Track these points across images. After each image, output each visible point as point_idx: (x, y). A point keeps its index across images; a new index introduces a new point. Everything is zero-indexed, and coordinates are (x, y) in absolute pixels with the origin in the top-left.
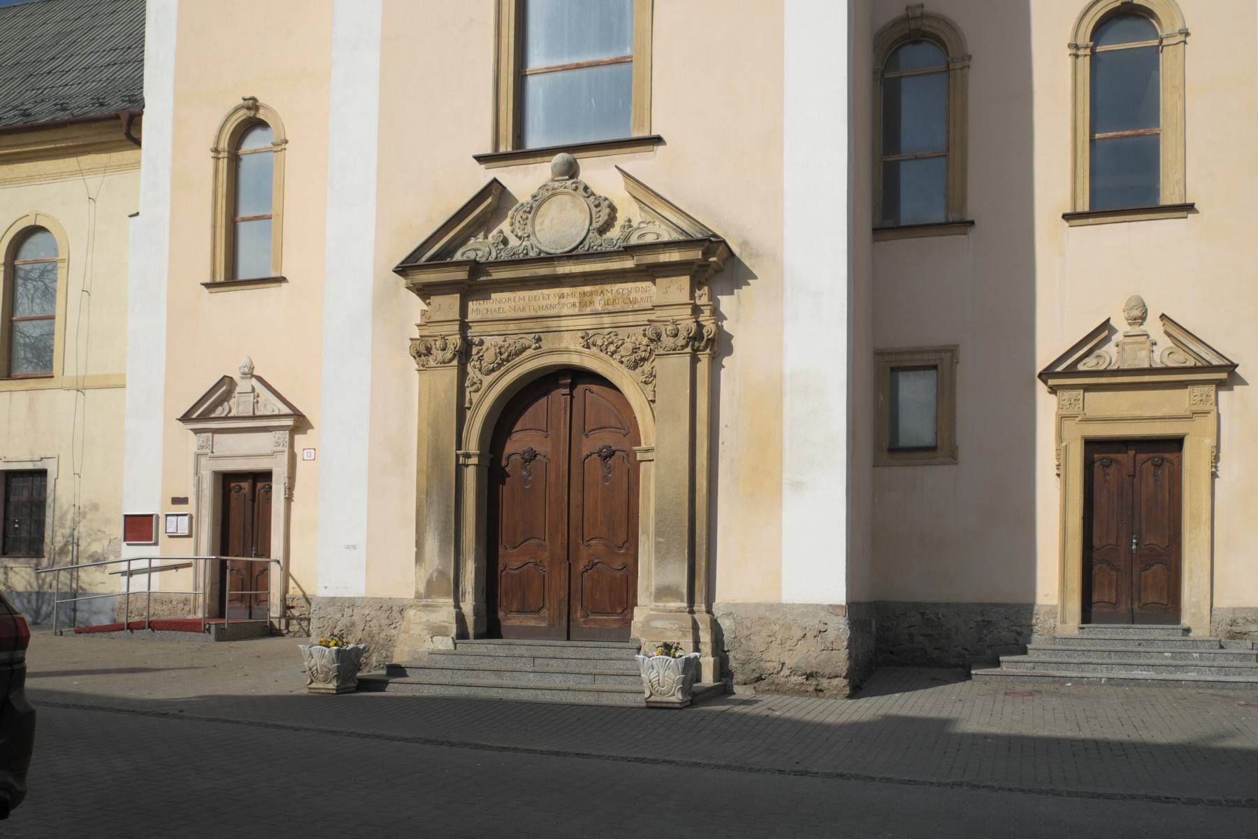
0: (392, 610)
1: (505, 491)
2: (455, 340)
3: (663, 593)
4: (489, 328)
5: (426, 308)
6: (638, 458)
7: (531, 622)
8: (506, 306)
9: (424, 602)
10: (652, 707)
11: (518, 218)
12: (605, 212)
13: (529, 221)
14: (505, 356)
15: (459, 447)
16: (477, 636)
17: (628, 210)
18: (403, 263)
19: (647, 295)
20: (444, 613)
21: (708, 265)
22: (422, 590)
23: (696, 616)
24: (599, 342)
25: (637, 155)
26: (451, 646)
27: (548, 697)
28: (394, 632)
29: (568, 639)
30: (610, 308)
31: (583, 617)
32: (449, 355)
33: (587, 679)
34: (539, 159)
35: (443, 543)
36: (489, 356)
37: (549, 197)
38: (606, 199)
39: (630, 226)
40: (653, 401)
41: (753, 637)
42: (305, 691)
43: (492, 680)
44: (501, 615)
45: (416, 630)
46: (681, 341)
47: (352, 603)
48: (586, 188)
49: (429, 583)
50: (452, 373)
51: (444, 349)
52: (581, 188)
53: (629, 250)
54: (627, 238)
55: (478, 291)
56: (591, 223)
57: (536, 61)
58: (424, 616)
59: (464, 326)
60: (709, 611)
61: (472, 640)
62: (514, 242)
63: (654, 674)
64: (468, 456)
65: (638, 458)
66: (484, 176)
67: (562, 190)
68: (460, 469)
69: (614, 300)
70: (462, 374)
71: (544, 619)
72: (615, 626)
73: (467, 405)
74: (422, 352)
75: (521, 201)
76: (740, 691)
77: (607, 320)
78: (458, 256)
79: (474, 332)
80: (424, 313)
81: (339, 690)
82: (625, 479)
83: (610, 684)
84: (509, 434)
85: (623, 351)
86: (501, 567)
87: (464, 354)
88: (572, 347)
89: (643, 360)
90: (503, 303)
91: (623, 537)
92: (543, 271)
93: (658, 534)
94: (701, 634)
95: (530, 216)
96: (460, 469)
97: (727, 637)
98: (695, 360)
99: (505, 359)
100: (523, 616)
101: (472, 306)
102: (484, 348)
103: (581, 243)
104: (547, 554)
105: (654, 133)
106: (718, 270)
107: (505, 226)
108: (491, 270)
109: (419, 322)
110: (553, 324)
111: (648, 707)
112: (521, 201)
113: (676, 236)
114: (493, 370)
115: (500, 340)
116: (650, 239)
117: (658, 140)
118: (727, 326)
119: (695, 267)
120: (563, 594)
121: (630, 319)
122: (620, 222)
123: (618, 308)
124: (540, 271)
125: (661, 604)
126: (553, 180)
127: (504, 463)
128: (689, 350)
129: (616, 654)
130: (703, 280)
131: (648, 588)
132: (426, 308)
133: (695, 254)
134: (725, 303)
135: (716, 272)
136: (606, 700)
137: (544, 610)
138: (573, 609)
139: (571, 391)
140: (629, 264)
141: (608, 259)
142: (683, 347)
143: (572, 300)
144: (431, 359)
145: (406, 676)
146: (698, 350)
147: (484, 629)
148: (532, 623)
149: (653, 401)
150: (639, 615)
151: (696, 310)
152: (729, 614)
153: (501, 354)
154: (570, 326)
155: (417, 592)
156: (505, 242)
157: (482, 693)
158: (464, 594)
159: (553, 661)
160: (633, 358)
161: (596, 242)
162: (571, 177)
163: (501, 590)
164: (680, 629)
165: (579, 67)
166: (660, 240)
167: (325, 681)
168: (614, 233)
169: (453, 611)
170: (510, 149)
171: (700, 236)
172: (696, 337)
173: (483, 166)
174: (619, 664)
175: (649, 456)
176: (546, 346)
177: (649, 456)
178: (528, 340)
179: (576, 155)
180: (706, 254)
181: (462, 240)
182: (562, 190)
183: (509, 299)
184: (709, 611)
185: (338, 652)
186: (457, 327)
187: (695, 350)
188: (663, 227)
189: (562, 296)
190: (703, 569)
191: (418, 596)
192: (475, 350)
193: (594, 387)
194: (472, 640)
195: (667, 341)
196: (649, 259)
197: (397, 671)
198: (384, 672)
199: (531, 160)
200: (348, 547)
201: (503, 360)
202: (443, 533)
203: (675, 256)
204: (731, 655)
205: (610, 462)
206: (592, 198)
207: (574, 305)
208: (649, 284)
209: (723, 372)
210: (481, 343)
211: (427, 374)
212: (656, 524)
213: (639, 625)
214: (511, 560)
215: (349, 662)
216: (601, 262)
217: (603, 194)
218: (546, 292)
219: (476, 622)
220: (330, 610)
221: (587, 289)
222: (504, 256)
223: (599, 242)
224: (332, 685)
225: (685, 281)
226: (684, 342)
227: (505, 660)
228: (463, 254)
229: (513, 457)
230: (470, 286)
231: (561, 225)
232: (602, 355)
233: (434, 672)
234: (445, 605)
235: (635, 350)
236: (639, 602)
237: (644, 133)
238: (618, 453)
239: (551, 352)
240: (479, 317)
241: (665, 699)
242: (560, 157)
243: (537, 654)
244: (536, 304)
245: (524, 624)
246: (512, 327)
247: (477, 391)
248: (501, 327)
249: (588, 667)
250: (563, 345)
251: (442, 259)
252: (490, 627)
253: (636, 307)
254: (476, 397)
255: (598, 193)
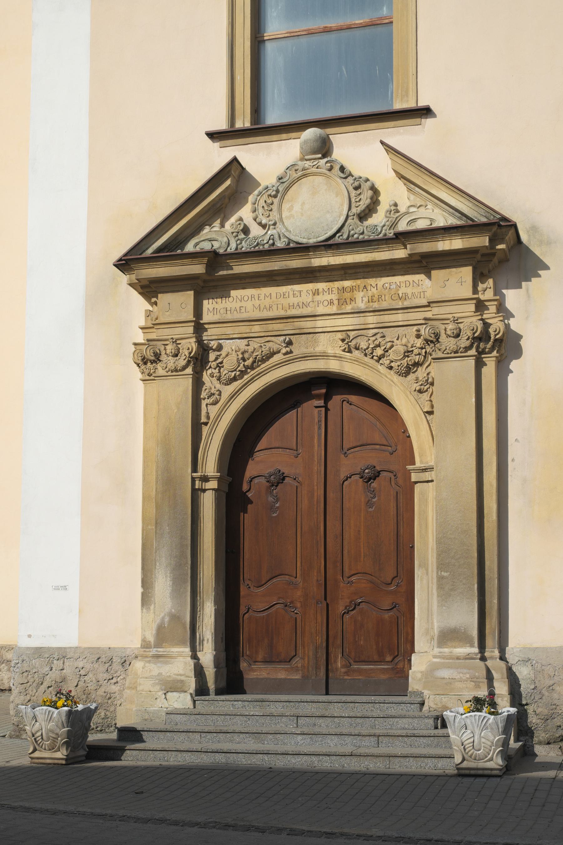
0: (114, 663)
1: (247, 520)
2: (190, 345)
3: (448, 636)
4: (229, 330)
5: (151, 309)
6: (413, 479)
7: (281, 673)
8: (249, 305)
9: (154, 651)
10: (464, 774)
11: (262, 202)
12: (367, 195)
13: (275, 207)
14: (248, 362)
15: (195, 469)
16: (219, 692)
17: (393, 192)
18: (126, 255)
19: (420, 289)
20: (180, 665)
21: (494, 254)
22: (151, 638)
23: (489, 663)
24: (363, 345)
25: (401, 130)
26: (190, 704)
27: (326, 764)
28: (114, 688)
29: (327, 693)
30: (376, 306)
31: (343, 666)
32: (182, 362)
33: (367, 742)
34: (284, 136)
35: (177, 582)
36: (230, 363)
37: (299, 179)
38: (367, 180)
39: (398, 211)
40: (431, 413)
41: (557, 688)
42: (25, 761)
43: (251, 744)
44: (243, 665)
45: (146, 685)
46: (463, 342)
47: (62, 654)
48: (342, 169)
49: (160, 629)
50: (185, 383)
51: (176, 355)
52: (337, 168)
53: (402, 238)
54: (394, 224)
55: (215, 287)
56: (350, 208)
57: (274, 26)
58: (155, 669)
59: (199, 328)
60: (502, 658)
61: (212, 696)
62: (256, 231)
63: (467, 735)
64: (205, 479)
65: (413, 479)
66: (220, 156)
67: (314, 170)
68: (196, 494)
69: (380, 297)
70: (198, 384)
71: (297, 669)
72: (383, 677)
73: (203, 419)
74: (148, 359)
75: (263, 184)
76: (544, 753)
77: (372, 319)
78: (190, 247)
79: (209, 335)
80: (148, 314)
81: (70, 761)
82: (393, 504)
83: (398, 748)
84: (251, 453)
85: (392, 355)
86: (243, 609)
87: (200, 360)
88: (330, 351)
89: (417, 364)
90: (244, 302)
91: (390, 572)
92: (296, 263)
93: (441, 566)
94: (496, 684)
95: (276, 201)
96: (196, 494)
97: (525, 688)
98: (479, 364)
99: (249, 366)
100: (270, 666)
101: (207, 305)
102: (223, 353)
103: (339, 231)
104: (299, 593)
105: (422, 103)
106: (504, 259)
107: (245, 213)
108: (232, 263)
109: (143, 324)
110: (307, 324)
111: (459, 775)
112: (263, 184)
113: (452, 221)
114: (235, 379)
115: (242, 344)
116: (421, 225)
117: (426, 112)
118: (514, 324)
119: (479, 256)
120: (320, 640)
121: (400, 317)
122: (382, 209)
123: (385, 305)
124: (290, 263)
125: (446, 650)
126: (302, 159)
127: (245, 487)
128: (473, 352)
129: (393, 710)
130: (486, 272)
131: (427, 632)
132: (151, 309)
133: (481, 241)
134: (513, 298)
135: (501, 262)
136: (398, 767)
137: (297, 659)
138: (332, 656)
139: (326, 402)
140: (400, 253)
141: (363, 252)
142: (467, 349)
143: (329, 297)
144: (159, 366)
145: (142, 741)
146: (483, 352)
147: (223, 684)
148: (282, 675)
149: (431, 413)
150: (419, 664)
151: (480, 306)
152: (526, 661)
153: (244, 360)
154: (328, 326)
155: (144, 640)
156: (246, 231)
157: (243, 761)
158: (202, 641)
159: (321, 720)
160: (404, 362)
161: (357, 230)
162: (324, 156)
163: (243, 637)
164: (472, 679)
165: (327, 30)
166: (434, 225)
167: (52, 748)
168: (378, 219)
169: (191, 662)
170: (248, 125)
171: (484, 220)
172: (482, 338)
173: (217, 145)
174: (402, 723)
175: (427, 476)
176: (297, 350)
177: (427, 476)
178: (277, 343)
179: (329, 131)
180: (493, 241)
181: (194, 229)
182: (314, 170)
183: (252, 297)
184: (502, 658)
185: (70, 713)
186: (191, 330)
187: (481, 352)
188: (437, 210)
189: (316, 292)
190: (496, 607)
191: (146, 645)
192: (212, 356)
193: (353, 398)
194: (212, 696)
195: (447, 343)
196: (425, 247)
197: (130, 735)
198: (114, 736)
199: (275, 137)
200: (57, 588)
201: (247, 367)
202: (177, 568)
203: (456, 243)
204: (530, 710)
205: (375, 484)
206: (350, 179)
207: (331, 302)
208: (422, 277)
209: (510, 377)
210: (220, 348)
211: (155, 385)
212: (439, 555)
213: (419, 675)
214: (255, 600)
215: (79, 722)
216: (358, 252)
217: (364, 175)
218: (297, 287)
219: (217, 674)
220: (36, 662)
221: (347, 284)
222: (245, 247)
223: (360, 229)
224: (61, 754)
225: (466, 272)
226: (468, 343)
227: (262, 720)
228: (196, 245)
229: (256, 481)
230: (205, 281)
231: (313, 212)
232: (367, 359)
233: (176, 736)
234: (180, 655)
235: (407, 353)
236: (416, 649)
237: (410, 104)
238: (383, 474)
239: (304, 357)
240: (216, 318)
241: (481, 765)
242: (311, 133)
243: (300, 712)
244: (285, 302)
245: (273, 676)
246: (257, 328)
247: (215, 403)
248: (244, 329)
249: (365, 727)
250: (319, 349)
251: (172, 251)
252: (232, 681)
253: (407, 304)
254: (214, 411)
255: (356, 173)
